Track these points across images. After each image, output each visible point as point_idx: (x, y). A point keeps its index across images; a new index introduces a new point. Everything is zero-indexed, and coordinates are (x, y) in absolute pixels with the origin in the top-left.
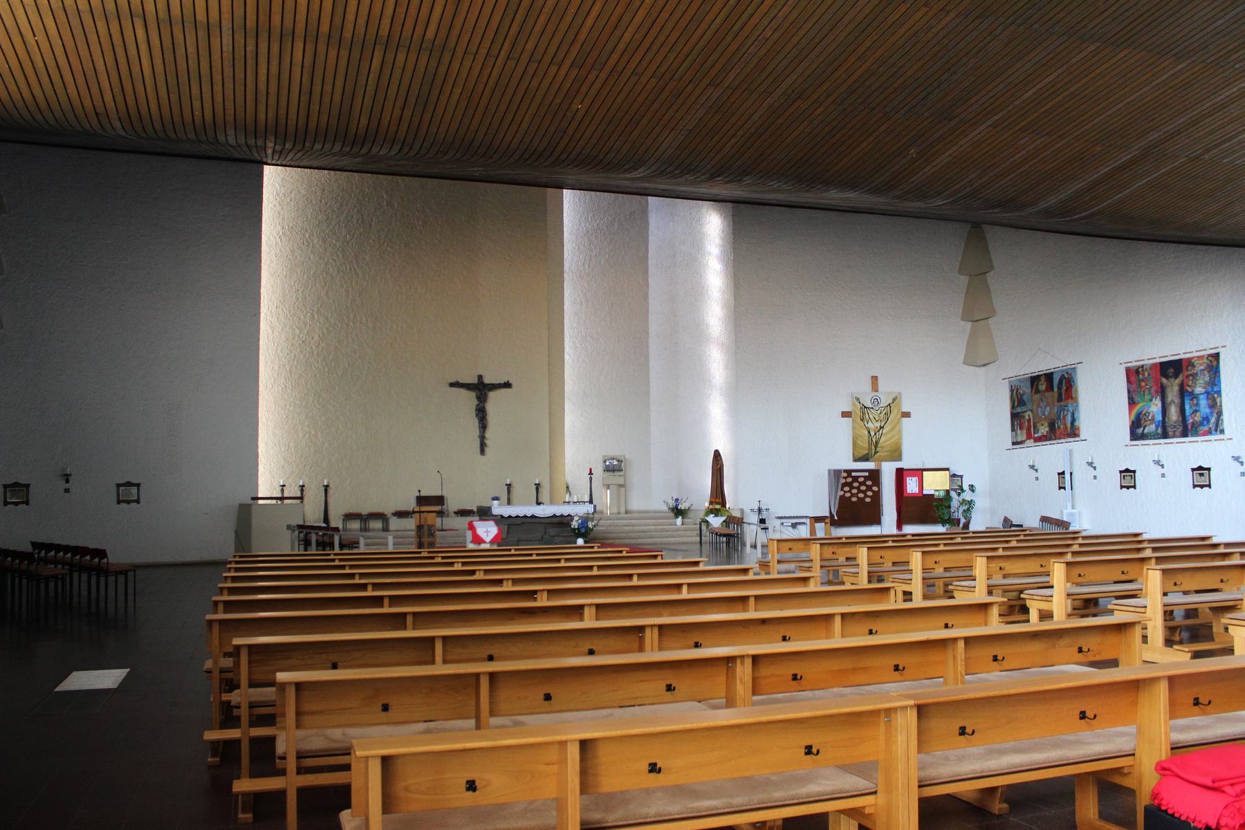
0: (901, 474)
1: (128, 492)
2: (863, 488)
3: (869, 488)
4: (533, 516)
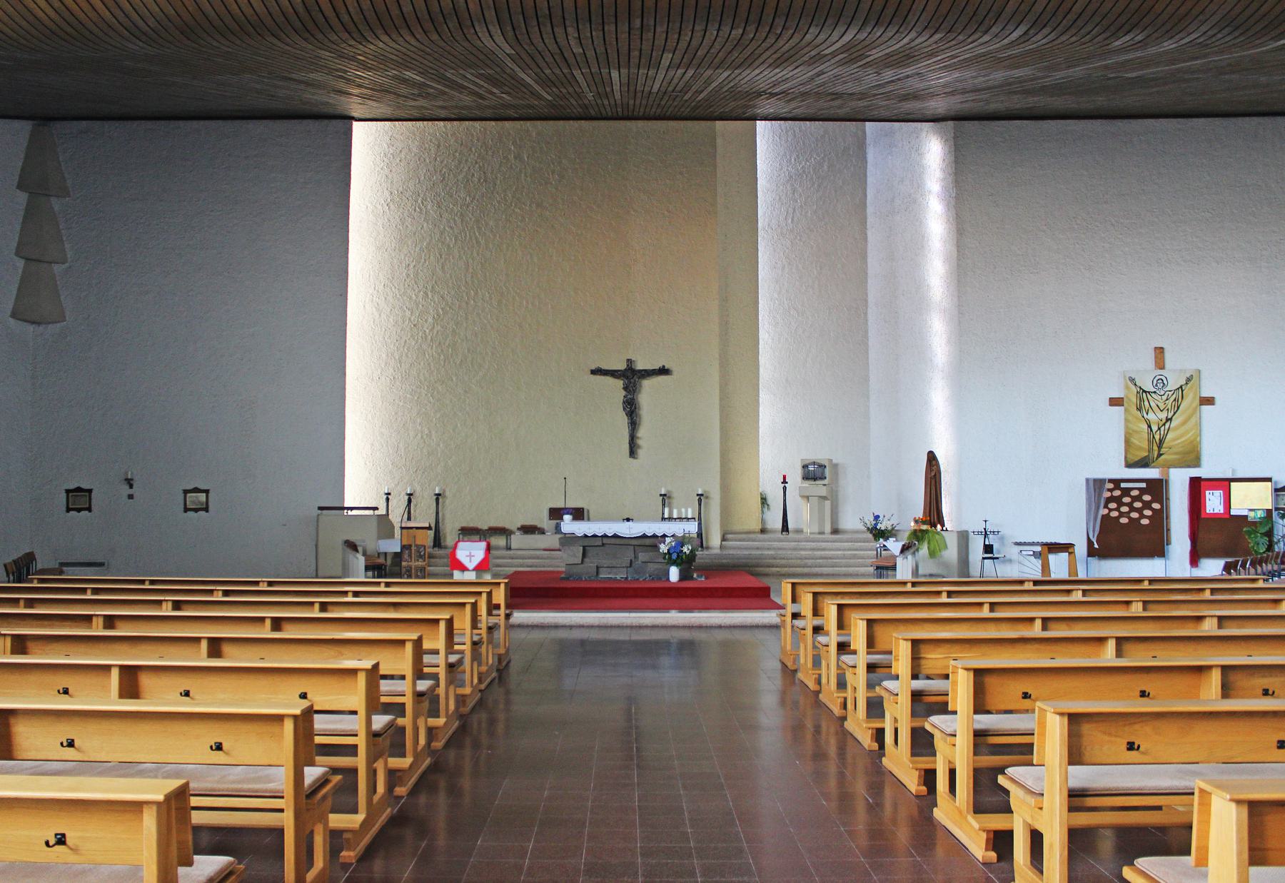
0: (1197, 487)
1: (196, 501)
2: (1138, 505)
3: (1147, 505)
4: (615, 536)
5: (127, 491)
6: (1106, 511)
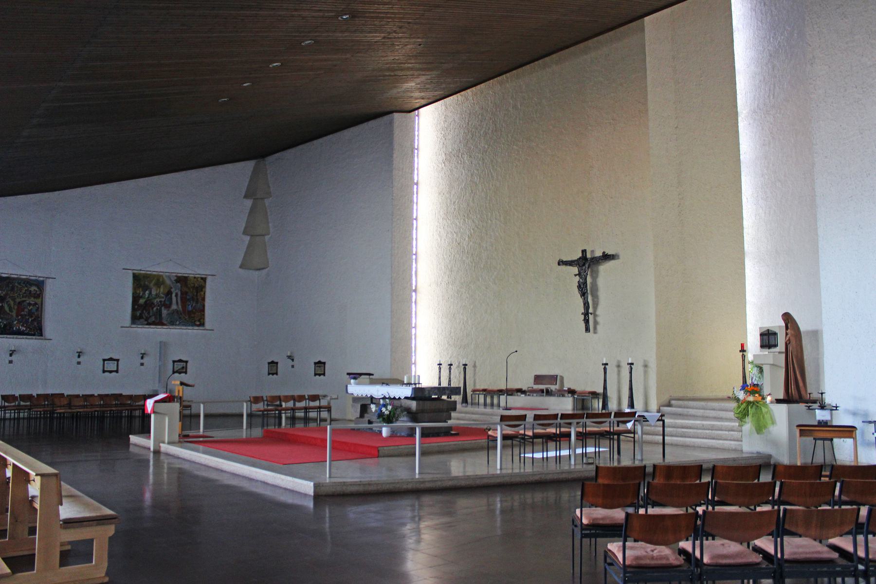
5: (292, 363)
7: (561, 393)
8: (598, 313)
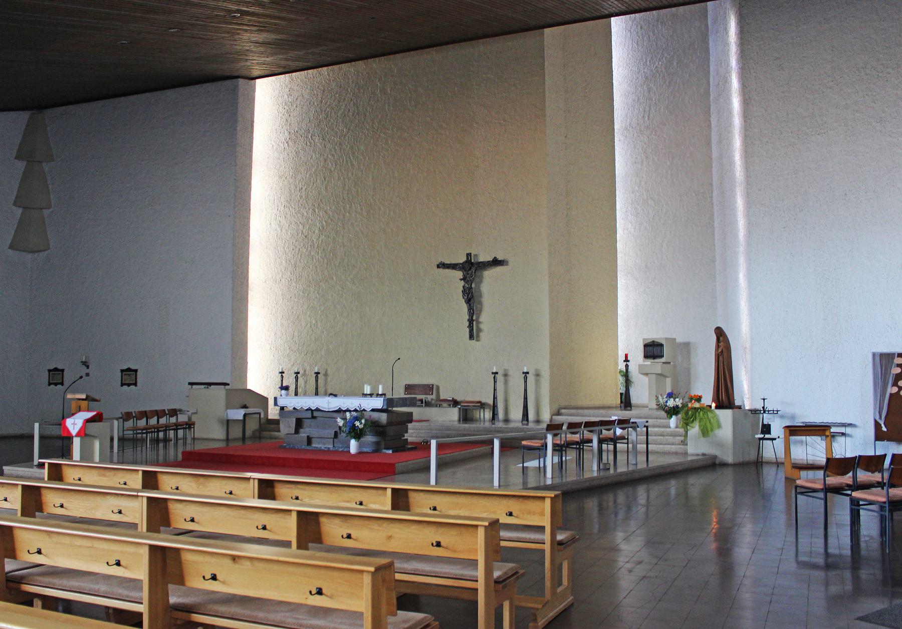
6: (895, 390)
7: (439, 403)
8: (481, 320)
